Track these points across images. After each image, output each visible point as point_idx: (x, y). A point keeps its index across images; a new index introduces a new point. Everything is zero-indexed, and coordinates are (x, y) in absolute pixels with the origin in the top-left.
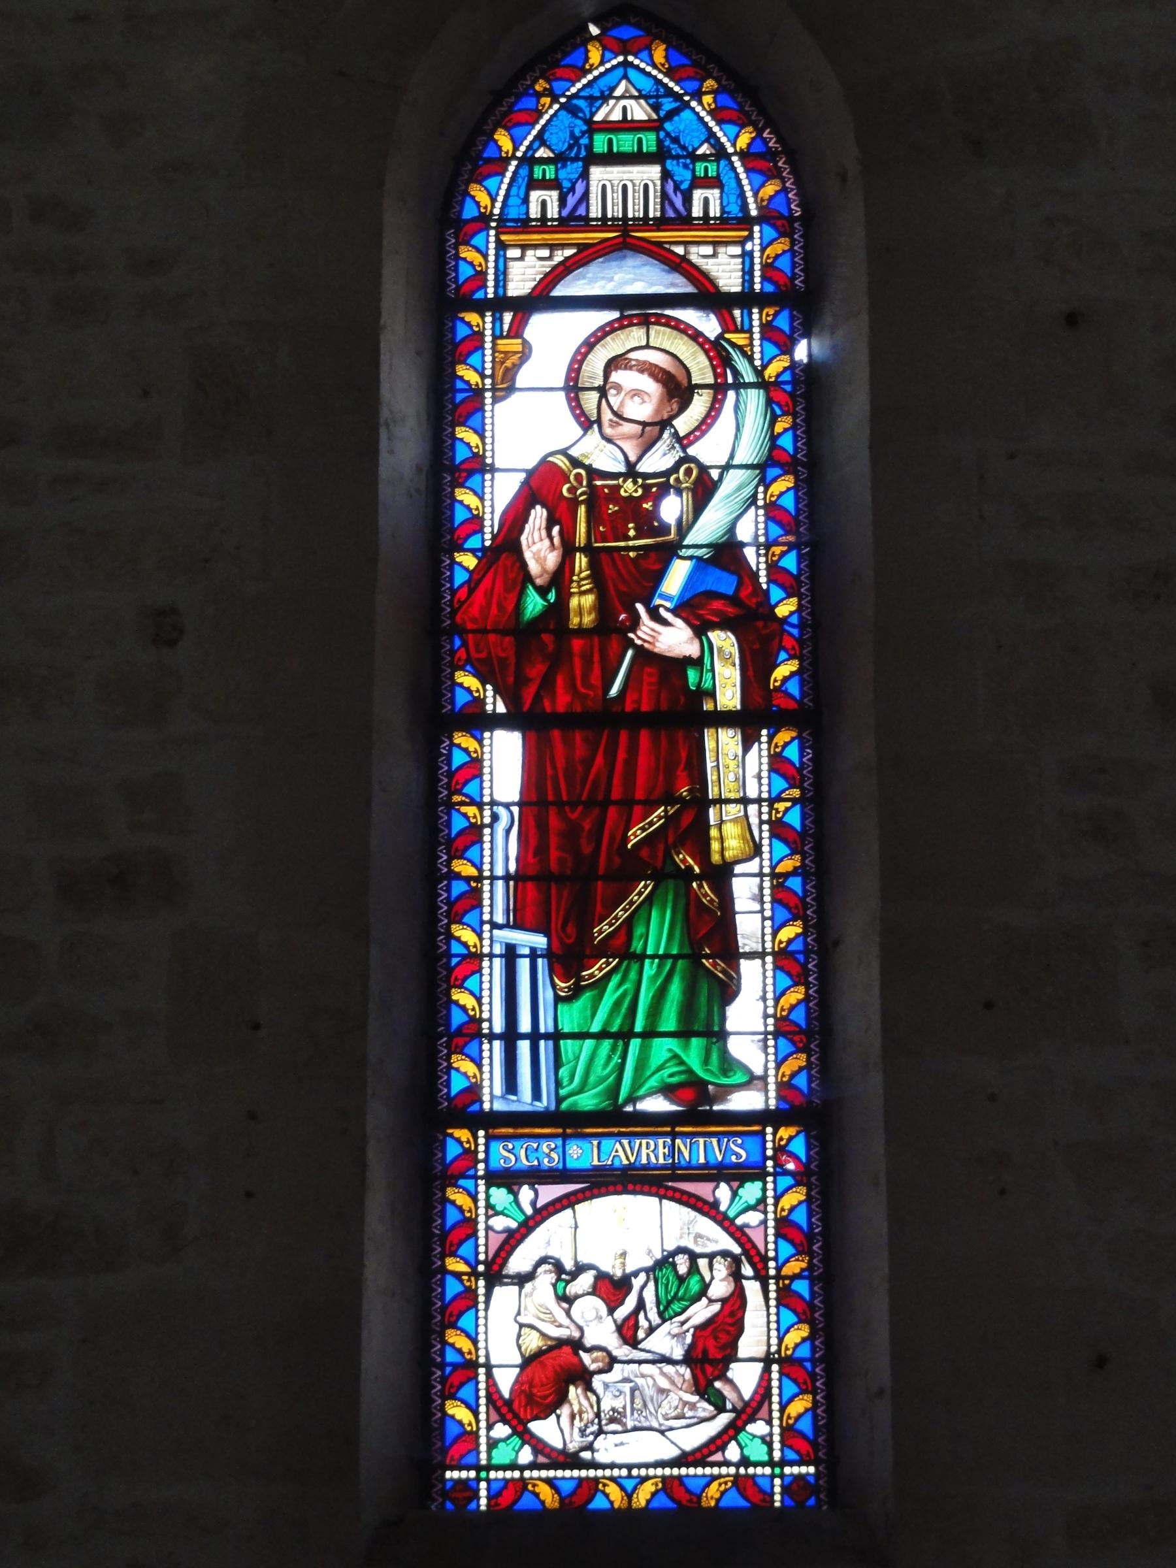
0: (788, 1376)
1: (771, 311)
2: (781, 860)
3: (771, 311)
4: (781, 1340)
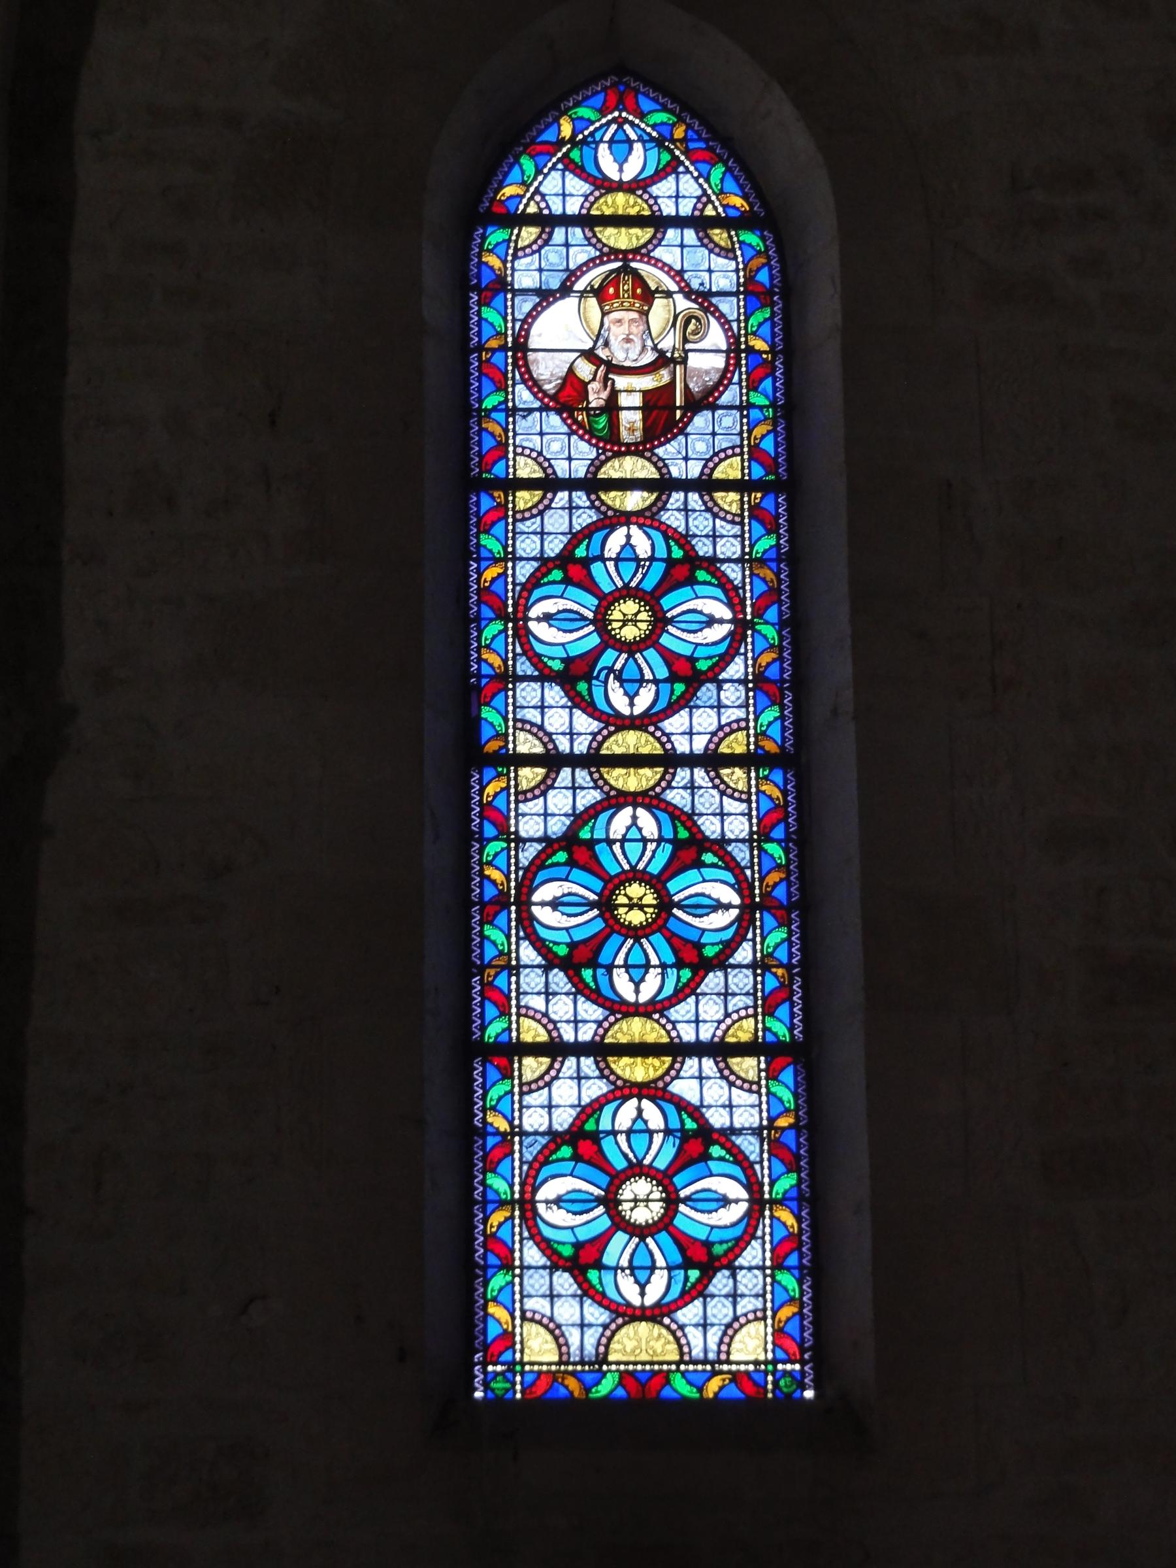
0: (776, 1156)
1: (759, 495)
2: (762, 653)
3: (759, 495)
4: (752, 546)
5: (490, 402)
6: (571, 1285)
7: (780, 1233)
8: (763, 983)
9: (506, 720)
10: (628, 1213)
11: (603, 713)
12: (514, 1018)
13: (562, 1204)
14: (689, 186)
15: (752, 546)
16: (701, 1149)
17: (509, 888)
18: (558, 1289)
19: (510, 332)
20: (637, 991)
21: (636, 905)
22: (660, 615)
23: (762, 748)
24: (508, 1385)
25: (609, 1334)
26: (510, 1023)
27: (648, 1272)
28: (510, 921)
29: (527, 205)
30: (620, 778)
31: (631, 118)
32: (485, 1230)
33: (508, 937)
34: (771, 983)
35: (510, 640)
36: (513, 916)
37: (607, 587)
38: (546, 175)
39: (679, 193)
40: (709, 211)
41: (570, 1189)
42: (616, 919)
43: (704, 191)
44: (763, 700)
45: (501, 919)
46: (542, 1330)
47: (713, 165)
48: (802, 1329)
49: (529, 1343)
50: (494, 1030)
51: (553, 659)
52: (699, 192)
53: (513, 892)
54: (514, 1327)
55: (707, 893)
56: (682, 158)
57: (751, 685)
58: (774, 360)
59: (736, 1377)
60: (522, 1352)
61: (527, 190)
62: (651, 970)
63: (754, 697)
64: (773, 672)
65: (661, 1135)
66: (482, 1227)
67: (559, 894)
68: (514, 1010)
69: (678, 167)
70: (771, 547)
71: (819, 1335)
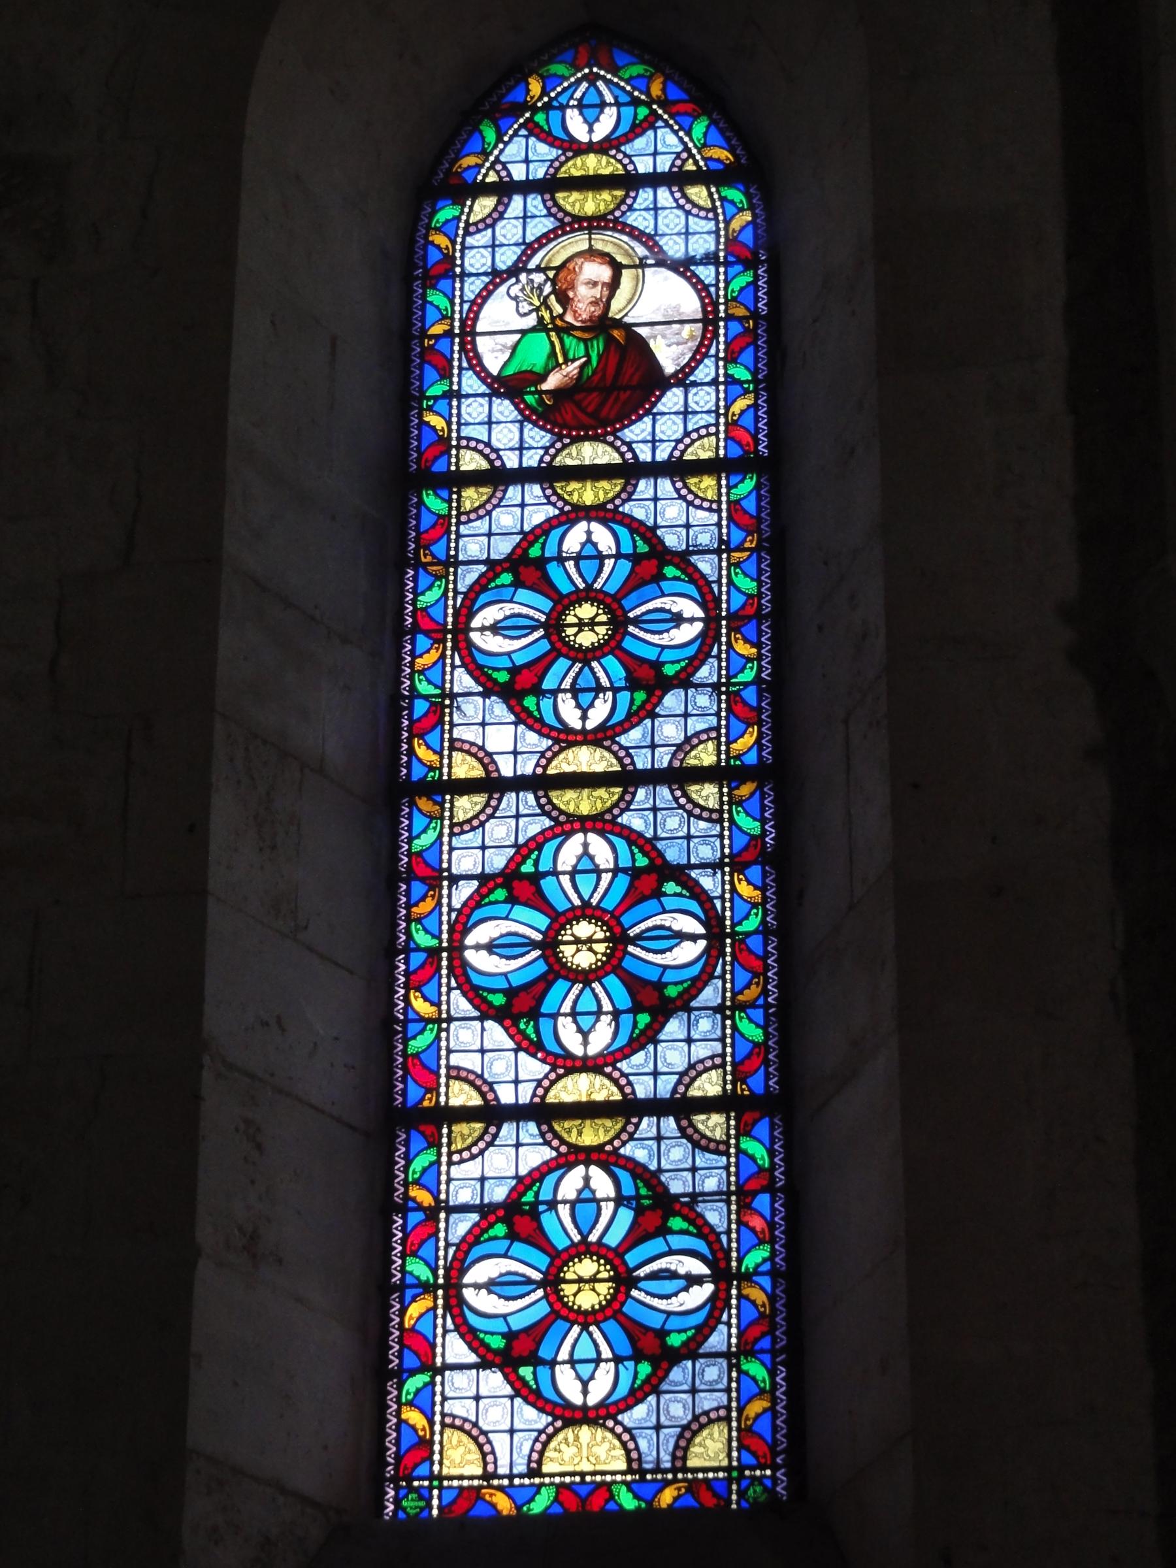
1: (426, 1103)
3: (426, 1103)
4: (438, 1038)
5: (436, 390)
6: (666, 244)
7: (750, 1314)
8: (449, 548)
9: (732, 821)
10: (571, 1298)
11: (619, 835)
12: (724, 499)
13: (493, 1288)
14: (669, 140)
15: (438, 1038)
16: (659, 1222)
17: (728, 635)
18: (681, 240)
19: (457, 316)
20: (585, 1392)
21: (584, 942)
22: (549, 952)
23: (435, 803)
24: (422, 1504)
25: (544, 1439)
26: (728, 494)
27: (593, 1365)
28: (728, 601)
29: (486, 175)
30: (571, 801)
31: (602, 73)
32: (401, 1323)
33: (730, 583)
34: (439, 549)
35: (728, 914)
36: (724, 606)
37: (612, 981)
38: (506, 144)
39: (656, 150)
40: (690, 166)
41: (504, 1271)
42: (608, 610)
43: (685, 144)
44: (430, 858)
45: (738, 601)
46: (465, 1438)
47: (696, 118)
48: (775, 1429)
49: (449, 1453)
50: (749, 485)
51: (676, 895)
52: (680, 148)
53: (724, 631)
54: (432, 1433)
55: (507, 640)
56: (660, 112)
57: (446, 874)
58: (756, 326)
59: (693, 1487)
60: (441, 1463)
61: (487, 160)
62: (603, 1017)
63: (441, 861)
64: (418, 888)
65: (611, 1205)
66: (398, 1320)
67: (673, 632)
68: (724, 506)
69: (656, 121)
70: (414, 1037)
71: (794, 1433)
